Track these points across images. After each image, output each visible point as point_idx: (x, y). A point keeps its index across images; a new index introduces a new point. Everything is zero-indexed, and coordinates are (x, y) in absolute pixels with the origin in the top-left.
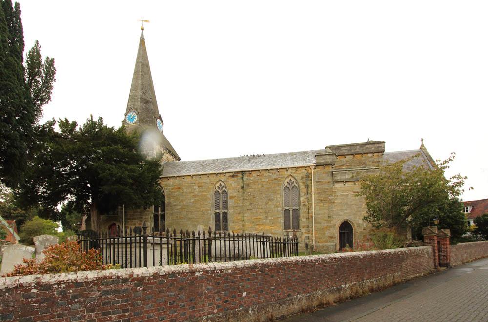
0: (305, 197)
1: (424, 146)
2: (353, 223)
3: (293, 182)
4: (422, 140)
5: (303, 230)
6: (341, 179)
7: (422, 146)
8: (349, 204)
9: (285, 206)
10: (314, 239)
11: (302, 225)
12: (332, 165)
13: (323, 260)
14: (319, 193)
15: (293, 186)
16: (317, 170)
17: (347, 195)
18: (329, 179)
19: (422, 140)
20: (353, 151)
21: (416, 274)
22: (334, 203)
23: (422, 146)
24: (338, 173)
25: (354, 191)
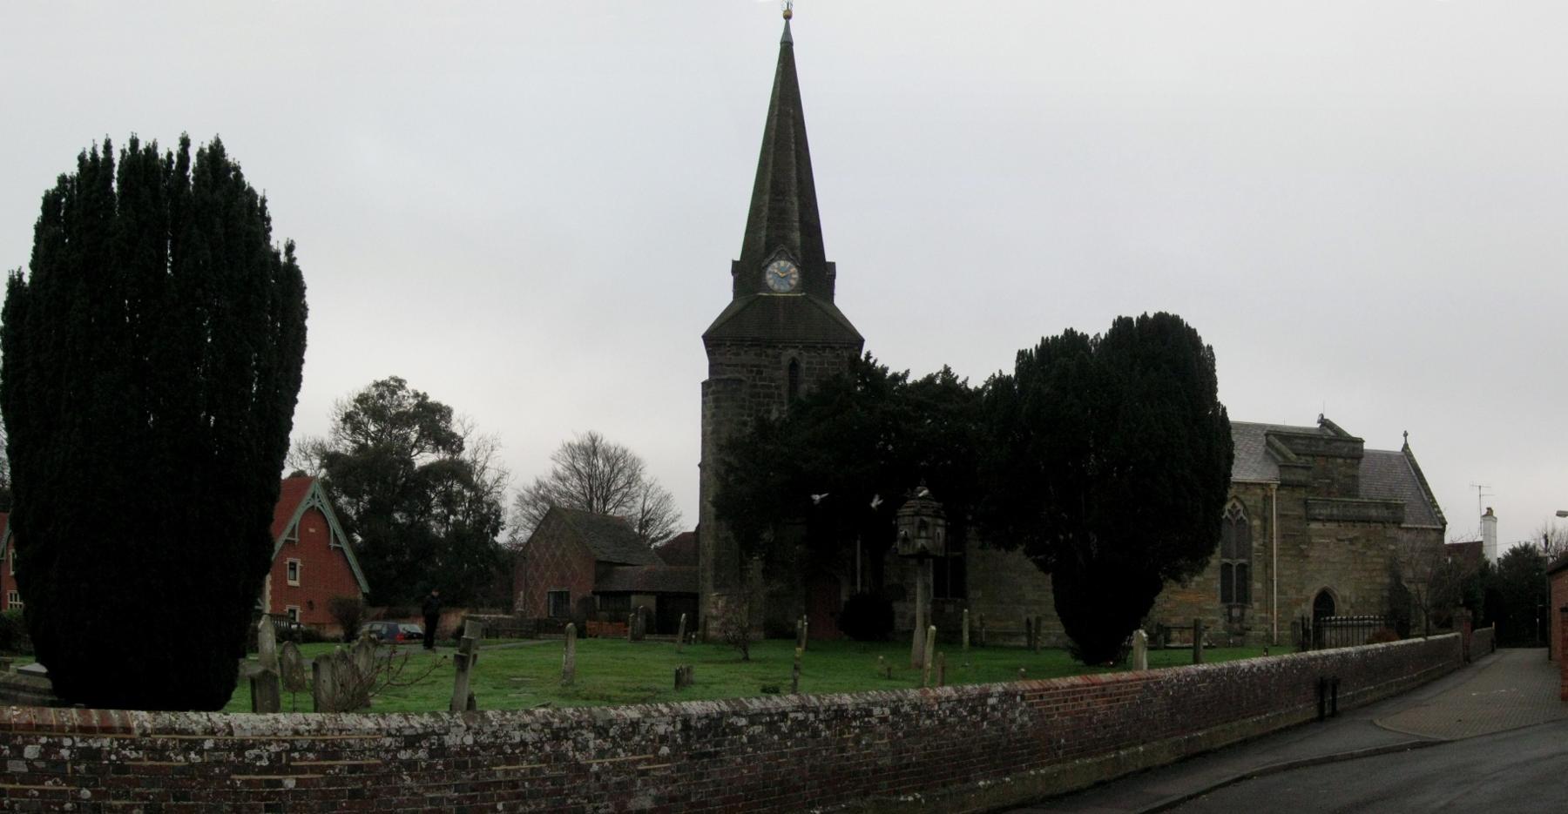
0: (1261, 541)
1: (1410, 447)
2: (1335, 595)
3: (1239, 511)
4: (1406, 435)
5: (1256, 605)
6: (1320, 514)
7: (1406, 446)
8: (1331, 560)
9: (1223, 557)
10: (1275, 622)
11: (1254, 595)
12: (1382, 522)
13: (156, 766)
14: (1284, 537)
15: (1239, 517)
16: (1282, 492)
17: (1327, 546)
18: (1300, 511)
19: (1406, 435)
20: (1313, 449)
21: (1136, 745)
22: (1308, 557)
23: (1406, 446)
24: (1315, 504)
25: (1339, 537)
